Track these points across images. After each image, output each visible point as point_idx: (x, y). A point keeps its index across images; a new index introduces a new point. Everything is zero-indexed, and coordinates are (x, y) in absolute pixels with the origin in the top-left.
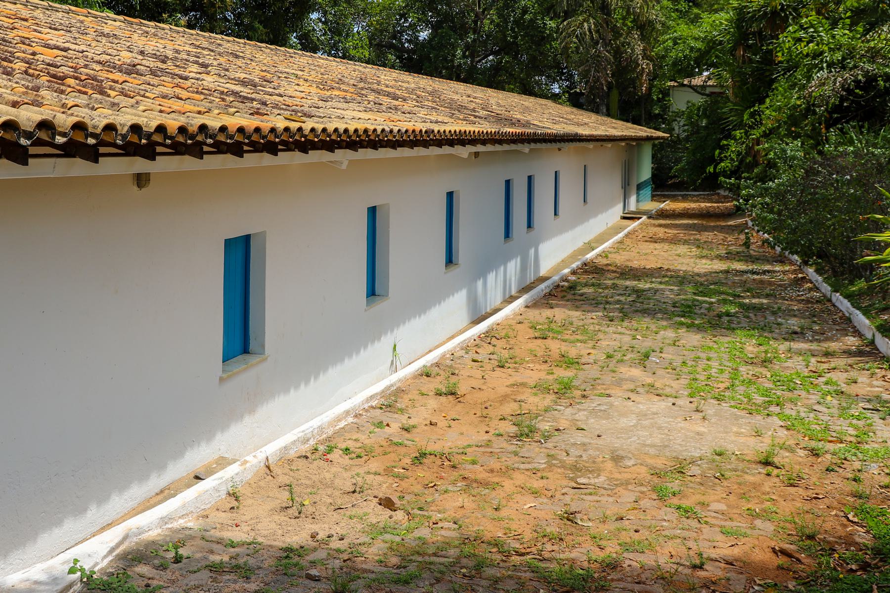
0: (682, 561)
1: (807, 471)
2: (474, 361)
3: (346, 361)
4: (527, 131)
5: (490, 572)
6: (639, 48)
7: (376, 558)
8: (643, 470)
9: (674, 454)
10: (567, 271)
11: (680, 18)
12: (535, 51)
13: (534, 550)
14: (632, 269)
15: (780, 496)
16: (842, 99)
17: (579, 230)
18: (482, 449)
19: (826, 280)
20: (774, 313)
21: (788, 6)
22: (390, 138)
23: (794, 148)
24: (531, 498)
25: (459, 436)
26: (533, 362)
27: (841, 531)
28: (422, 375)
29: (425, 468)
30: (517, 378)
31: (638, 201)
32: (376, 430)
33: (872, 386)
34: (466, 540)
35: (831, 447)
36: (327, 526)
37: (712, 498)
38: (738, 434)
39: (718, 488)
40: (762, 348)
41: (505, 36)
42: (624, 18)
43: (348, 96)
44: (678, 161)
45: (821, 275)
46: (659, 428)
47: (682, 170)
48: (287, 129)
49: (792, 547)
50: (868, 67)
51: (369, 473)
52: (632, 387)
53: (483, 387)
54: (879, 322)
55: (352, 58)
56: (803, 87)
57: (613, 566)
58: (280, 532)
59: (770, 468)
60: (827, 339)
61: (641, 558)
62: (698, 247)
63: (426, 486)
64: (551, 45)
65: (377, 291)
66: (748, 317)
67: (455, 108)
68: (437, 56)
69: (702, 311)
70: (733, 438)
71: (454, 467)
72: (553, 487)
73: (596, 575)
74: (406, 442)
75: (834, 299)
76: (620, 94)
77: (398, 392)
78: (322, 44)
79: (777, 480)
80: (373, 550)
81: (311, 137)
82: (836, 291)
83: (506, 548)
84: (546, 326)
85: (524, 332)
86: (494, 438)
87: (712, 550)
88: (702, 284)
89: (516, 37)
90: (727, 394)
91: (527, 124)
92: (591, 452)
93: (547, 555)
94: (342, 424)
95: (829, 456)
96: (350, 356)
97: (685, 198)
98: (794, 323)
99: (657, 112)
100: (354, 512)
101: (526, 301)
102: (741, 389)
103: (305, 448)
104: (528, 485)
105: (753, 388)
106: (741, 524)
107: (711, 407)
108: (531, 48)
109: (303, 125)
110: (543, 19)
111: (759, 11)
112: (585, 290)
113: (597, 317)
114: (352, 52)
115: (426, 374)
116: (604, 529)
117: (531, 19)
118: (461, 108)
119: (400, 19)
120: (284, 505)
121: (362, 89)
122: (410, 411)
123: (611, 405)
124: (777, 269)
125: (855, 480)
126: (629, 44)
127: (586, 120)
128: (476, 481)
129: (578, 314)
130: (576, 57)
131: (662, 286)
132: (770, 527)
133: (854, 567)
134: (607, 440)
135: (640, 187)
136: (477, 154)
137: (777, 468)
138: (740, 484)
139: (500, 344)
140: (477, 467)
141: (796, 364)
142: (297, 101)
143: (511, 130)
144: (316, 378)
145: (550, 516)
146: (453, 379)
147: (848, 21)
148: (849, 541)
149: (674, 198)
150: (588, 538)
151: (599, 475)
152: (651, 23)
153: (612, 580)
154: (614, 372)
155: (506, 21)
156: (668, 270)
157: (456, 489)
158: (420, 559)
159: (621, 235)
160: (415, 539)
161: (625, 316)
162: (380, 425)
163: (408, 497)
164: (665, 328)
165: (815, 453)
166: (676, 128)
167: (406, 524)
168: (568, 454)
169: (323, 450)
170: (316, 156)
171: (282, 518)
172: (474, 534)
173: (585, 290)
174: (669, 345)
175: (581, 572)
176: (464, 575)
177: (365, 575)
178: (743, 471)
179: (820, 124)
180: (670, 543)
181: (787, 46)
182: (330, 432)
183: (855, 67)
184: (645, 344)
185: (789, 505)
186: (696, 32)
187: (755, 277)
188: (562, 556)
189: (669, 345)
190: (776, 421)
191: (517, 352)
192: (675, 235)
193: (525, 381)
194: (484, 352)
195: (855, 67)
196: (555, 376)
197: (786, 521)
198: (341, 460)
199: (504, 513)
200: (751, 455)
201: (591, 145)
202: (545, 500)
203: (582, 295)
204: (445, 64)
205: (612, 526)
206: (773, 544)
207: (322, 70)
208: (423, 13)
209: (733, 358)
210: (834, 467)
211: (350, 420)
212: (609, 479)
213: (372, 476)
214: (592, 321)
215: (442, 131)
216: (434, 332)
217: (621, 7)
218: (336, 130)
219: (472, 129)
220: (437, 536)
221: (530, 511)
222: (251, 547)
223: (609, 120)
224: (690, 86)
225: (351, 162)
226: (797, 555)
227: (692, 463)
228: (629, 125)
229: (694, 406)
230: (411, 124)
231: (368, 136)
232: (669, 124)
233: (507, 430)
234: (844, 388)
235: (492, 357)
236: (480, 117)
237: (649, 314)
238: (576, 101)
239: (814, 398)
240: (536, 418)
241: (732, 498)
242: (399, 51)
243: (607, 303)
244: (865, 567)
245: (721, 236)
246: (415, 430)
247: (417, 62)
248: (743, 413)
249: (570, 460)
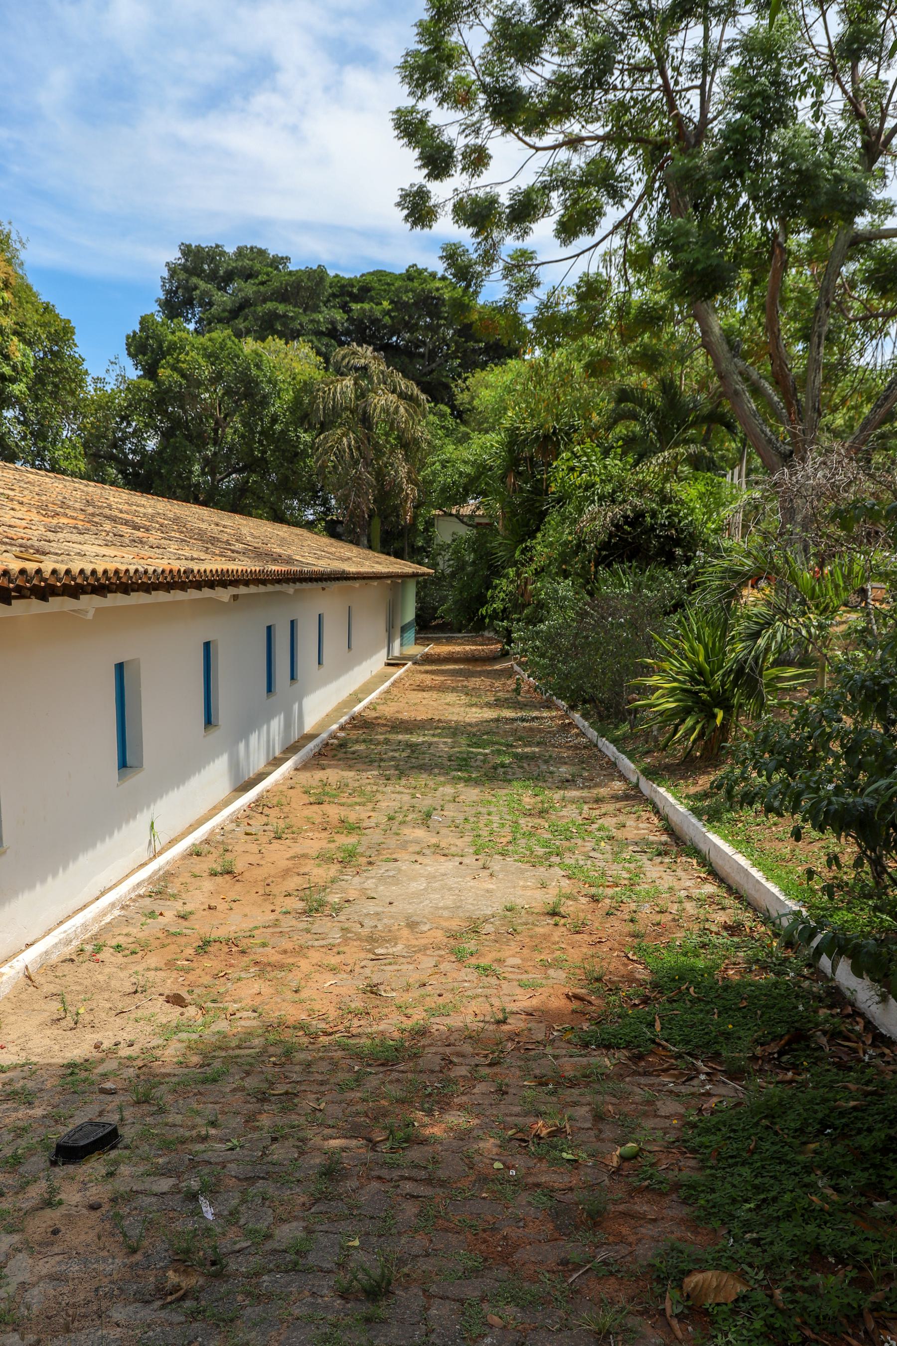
0: (487, 1019)
1: (589, 917)
2: (247, 834)
3: (98, 845)
4: (294, 568)
5: (301, 1056)
6: (403, 471)
7: (175, 1060)
8: (439, 934)
9: (468, 914)
10: (335, 727)
11: (447, 436)
12: (288, 469)
13: (341, 1027)
14: (402, 722)
15: (568, 944)
16: (611, 535)
17: (342, 680)
18: (270, 930)
19: (592, 725)
20: (546, 762)
21: (560, 430)
22: (145, 580)
23: (565, 588)
24: (329, 975)
25: (243, 918)
26: (311, 830)
27: (623, 970)
28: (191, 855)
29: (212, 957)
30: (297, 849)
31: (402, 645)
32: (149, 921)
33: (638, 828)
34: (268, 1028)
35: (610, 892)
36: (110, 1033)
37: (508, 953)
38: (525, 888)
39: (512, 943)
40: (539, 799)
41: (252, 450)
42: (387, 434)
43: (80, 524)
44: (443, 600)
45: (587, 720)
46: (450, 889)
47: (449, 610)
48: (23, 572)
49: (583, 991)
50: (637, 501)
51: (148, 969)
52: (418, 849)
53: (262, 862)
54: (643, 765)
55: (64, 472)
56: (575, 521)
57: (422, 1032)
58: (57, 1047)
59: (557, 918)
60: (597, 785)
61: (448, 1021)
62: (467, 694)
63: (216, 977)
64: (305, 463)
65: (128, 764)
66: (522, 767)
67: (209, 541)
68: (170, 472)
69: (478, 763)
70: (521, 892)
71: (243, 952)
72: (350, 961)
73: (407, 1044)
74: (184, 931)
75: (600, 745)
76: (382, 522)
77: (167, 876)
78: (23, 451)
79: (564, 929)
80: (170, 1051)
81: (52, 581)
82: (603, 736)
83: (312, 1030)
84: (320, 790)
85: (298, 799)
86: (281, 917)
87: (513, 1004)
88: (474, 735)
89: (264, 452)
90: (510, 848)
91: (289, 561)
92: (385, 921)
93: (355, 1031)
94: (108, 919)
95: (608, 901)
96: (103, 840)
97: (449, 641)
98: (564, 771)
99: (420, 544)
100: (139, 1013)
101: (295, 763)
102: (522, 842)
103: (68, 951)
104: (325, 962)
105: (533, 841)
106: (535, 976)
107: (496, 863)
108: (282, 465)
109: (41, 566)
110: (295, 430)
111: (532, 433)
112: (357, 747)
113: (373, 776)
114: (64, 464)
115: (195, 853)
116: (408, 998)
117: (282, 431)
118: (214, 540)
119: (122, 422)
120: (55, 1017)
121: (93, 515)
122: (184, 896)
123: (400, 870)
124: (545, 715)
125: (632, 921)
126: (392, 465)
127: (348, 554)
128: (269, 964)
129: (351, 774)
130: (333, 479)
131: (436, 739)
132: (562, 975)
133: (637, 1002)
134: (399, 906)
135: (404, 629)
136: (235, 597)
137: (564, 917)
138: (531, 937)
139: (273, 813)
140: (268, 949)
141: (570, 813)
142: (21, 533)
143: (274, 568)
144: (65, 868)
145: (352, 992)
146: (229, 857)
147: (619, 451)
148: (630, 979)
149: (438, 641)
150: (394, 1008)
151: (396, 944)
152: (416, 441)
153: (424, 1047)
154: (398, 834)
155: (252, 432)
156: (439, 721)
157: (249, 975)
158: (223, 1054)
159: (387, 684)
160: (214, 1034)
161: (402, 774)
162: (152, 914)
163: (197, 991)
164: (443, 784)
165: (595, 899)
166: (441, 563)
167: (200, 1020)
168: (362, 926)
169: (91, 950)
170: (57, 604)
171: (55, 1031)
172: (276, 1021)
173: (357, 747)
174: (449, 801)
175: (391, 1043)
176: (275, 1064)
177: (167, 1080)
178: (533, 924)
179: (590, 562)
180: (473, 1003)
181: (561, 474)
182: (95, 929)
183: (624, 501)
184: (425, 802)
185: (577, 952)
186: (467, 455)
187: (525, 724)
188: (369, 1030)
189: (449, 801)
190: (558, 872)
191: (292, 820)
192: (442, 682)
193: (305, 851)
194: (257, 823)
195: (624, 501)
196: (337, 844)
197: (576, 967)
198: (113, 959)
199: (304, 994)
200: (538, 907)
201: (357, 584)
202: (345, 976)
203: (353, 753)
204: (180, 482)
205: (416, 993)
206: (566, 990)
207: (37, 489)
208: (150, 416)
209: (512, 810)
210: (613, 910)
211: (117, 912)
212: (407, 946)
213: (152, 973)
214: (368, 781)
215: (202, 570)
216: (195, 804)
217: (384, 421)
218: (82, 571)
219: (235, 568)
220: (237, 1027)
221: (331, 989)
222: (26, 1068)
223: (371, 553)
224: (457, 516)
225: (98, 611)
226: (588, 998)
227: (486, 921)
228: (392, 559)
229: (480, 863)
230: (165, 561)
231: (119, 578)
232: (433, 559)
233: (294, 906)
234: (614, 832)
235: (266, 828)
236: (238, 552)
237: (425, 770)
238: (333, 531)
239: (589, 845)
240: (324, 890)
241: (525, 951)
242: (122, 464)
243: (381, 760)
244: (646, 1001)
245: (488, 682)
246: (192, 917)
247: (144, 478)
248: (527, 866)
249: (365, 932)
